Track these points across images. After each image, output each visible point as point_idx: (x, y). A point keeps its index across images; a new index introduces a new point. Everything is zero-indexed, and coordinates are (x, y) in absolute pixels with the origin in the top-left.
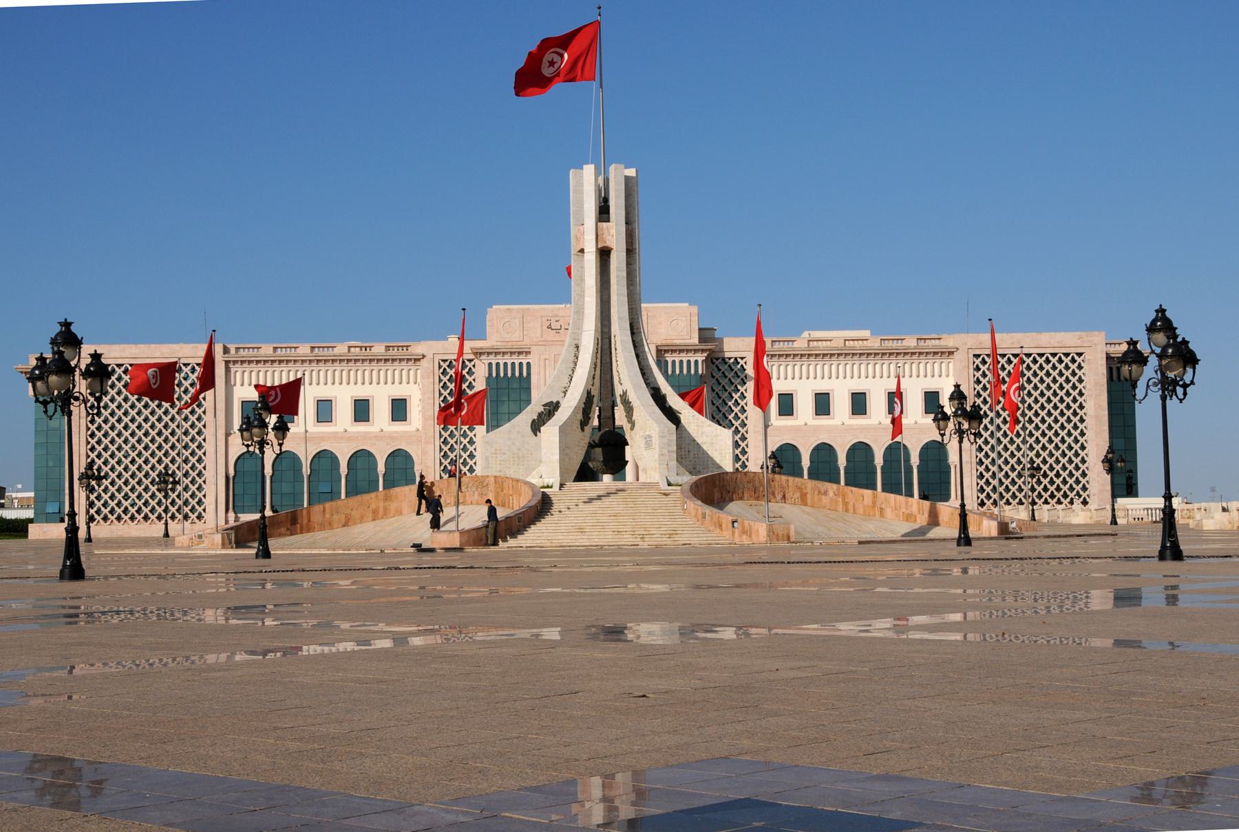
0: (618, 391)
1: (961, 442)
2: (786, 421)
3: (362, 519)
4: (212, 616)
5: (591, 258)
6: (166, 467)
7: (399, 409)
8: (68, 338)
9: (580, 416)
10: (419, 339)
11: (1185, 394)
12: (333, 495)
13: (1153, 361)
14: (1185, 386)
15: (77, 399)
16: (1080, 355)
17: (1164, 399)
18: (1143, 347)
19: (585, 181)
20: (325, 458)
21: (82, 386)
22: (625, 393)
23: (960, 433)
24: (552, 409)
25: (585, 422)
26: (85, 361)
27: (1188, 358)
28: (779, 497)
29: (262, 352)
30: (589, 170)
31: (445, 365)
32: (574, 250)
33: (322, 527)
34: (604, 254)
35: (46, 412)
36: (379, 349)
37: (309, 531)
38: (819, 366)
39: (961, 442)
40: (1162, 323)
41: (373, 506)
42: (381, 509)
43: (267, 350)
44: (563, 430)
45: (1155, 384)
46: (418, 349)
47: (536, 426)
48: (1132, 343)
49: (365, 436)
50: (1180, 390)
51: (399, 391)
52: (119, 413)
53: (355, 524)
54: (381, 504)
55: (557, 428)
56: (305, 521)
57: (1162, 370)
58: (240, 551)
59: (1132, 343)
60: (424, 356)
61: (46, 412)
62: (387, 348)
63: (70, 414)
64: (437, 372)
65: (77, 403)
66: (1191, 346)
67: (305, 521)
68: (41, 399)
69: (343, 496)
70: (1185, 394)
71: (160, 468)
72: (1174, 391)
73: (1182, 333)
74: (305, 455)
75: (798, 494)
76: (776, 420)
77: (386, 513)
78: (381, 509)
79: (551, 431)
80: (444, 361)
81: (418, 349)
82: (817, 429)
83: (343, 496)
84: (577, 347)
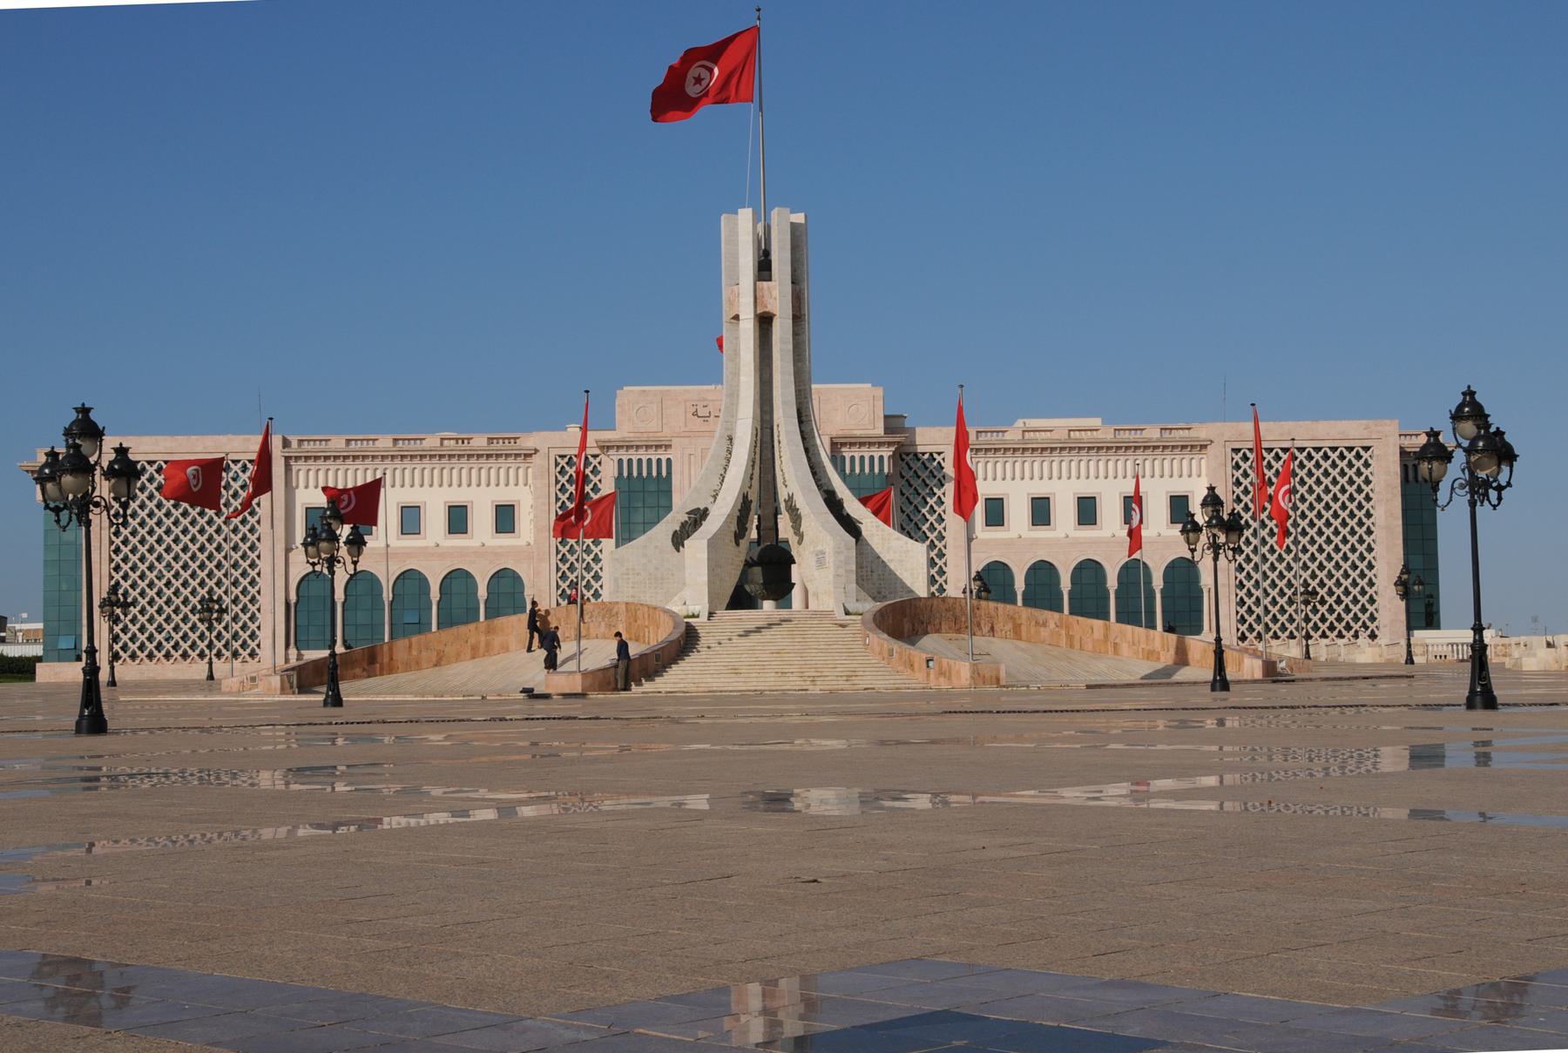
0: (783, 494)
1: (1216, 559)
2: (995, 533)
3: (458, 658)
4: (268, 780)
5: (748, 326)
6: (210, 592)
7: (505, 518)
8: (86, 428)
9: (734, 527)
10: (529, 429)
11: (1500, 499)
12: (422, 626)
13: (1459, 457)
14: (1500, 489)
15: (97, 505)
16: (1366, 449)
17: (1473, 504)
18: (1447, 439)
19: (740, 230)
20: (411, 580)
21: (103, 488)
22: (791, 498)
23: (1215, 548)
24: (698, 517)
25: (740, 534)
26: (108, 456)
27: (1504, 453)
28: (986, 629)
29: (331, 445)
30: (745, 216)
31: (563, 462)
32: (726, 317)
33: (407, 668)
34: (764, 322)
35: (58, 521)
36: (479, 442)
37: (391, 672)
38: (1037, 464)
39: (1216, 559)
40: (1470, 409)
41: (472, 640)
42: (482, 645)
43: (337, 443)
44: (713, 544)
45: (1462, 487)
46: (528, 441)
47: (678, 540)
48: (1433, 434)
49: (462, 552)
50: (1493, 494)
51: (505, 495)
52: (151, 523)
53: (449, 663)
54: (483, 638)
55: (705, 542)
56: (386, 660)
57: (1470, 468)
58: (303, 698)
59: (1433, 434)
60: (536, 451)
61: (58, 521)
62: (490, 440)
63: (88, 524)
64: (554, 471)
65: (97, 510)
66: (1507, 438)
67: (386, 660)
68: (52, 505)
69: (434, 628)
70: (1500, 499)
71: (203, 592)
72: (1486, 494)
73: (1496, 422)
74: (386, 576)
75: (1009, 626)
76: (982, 531)
77: (488, 650)
78: (482, 645)
79: (697, 546)
80: (562, 457)
81: (528, 441)
82: (1035, 542)
83: (434, 628)
84: (731, 439)
